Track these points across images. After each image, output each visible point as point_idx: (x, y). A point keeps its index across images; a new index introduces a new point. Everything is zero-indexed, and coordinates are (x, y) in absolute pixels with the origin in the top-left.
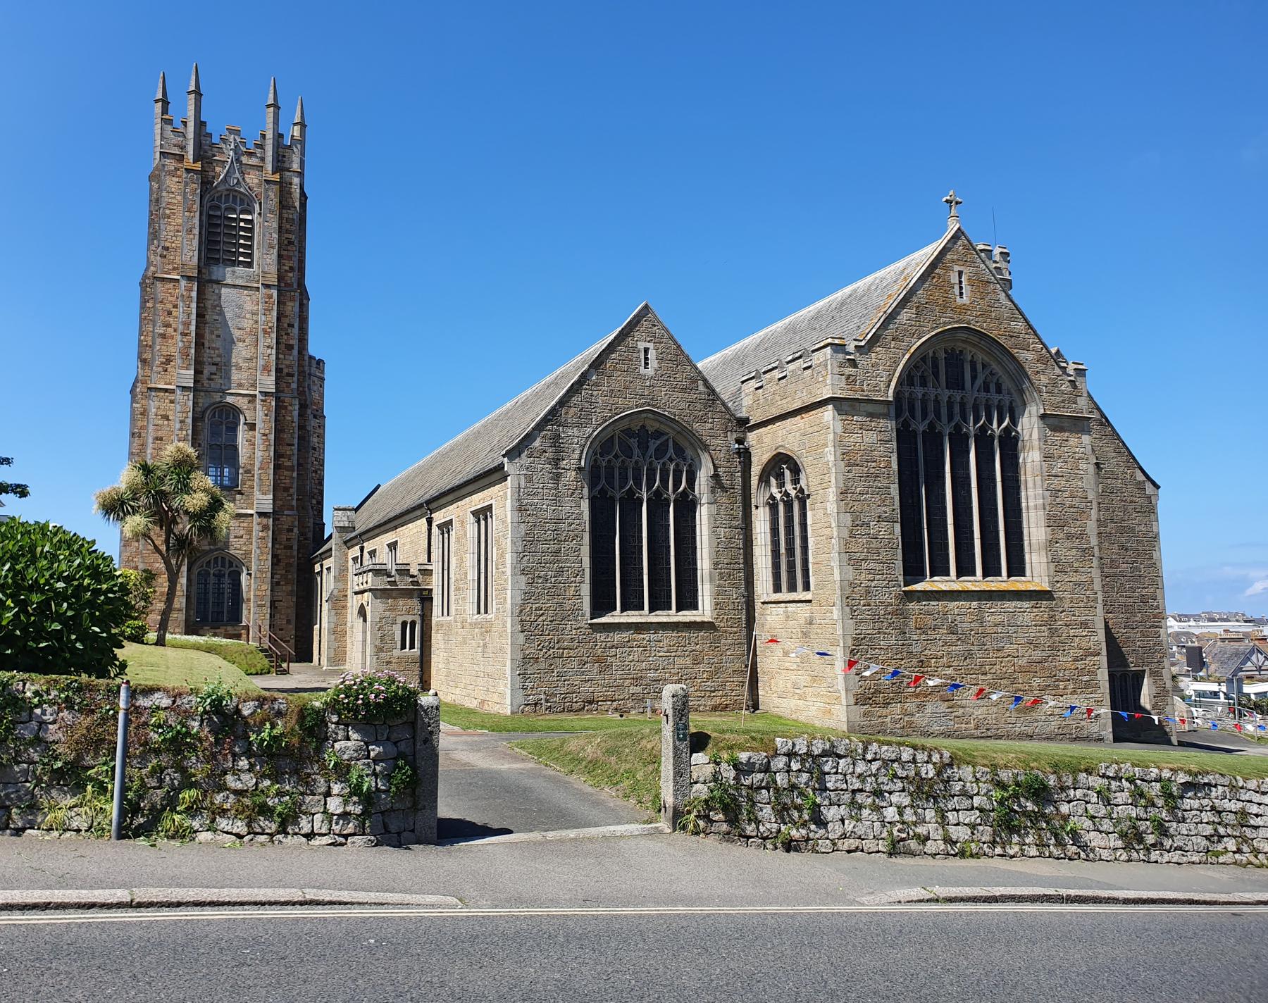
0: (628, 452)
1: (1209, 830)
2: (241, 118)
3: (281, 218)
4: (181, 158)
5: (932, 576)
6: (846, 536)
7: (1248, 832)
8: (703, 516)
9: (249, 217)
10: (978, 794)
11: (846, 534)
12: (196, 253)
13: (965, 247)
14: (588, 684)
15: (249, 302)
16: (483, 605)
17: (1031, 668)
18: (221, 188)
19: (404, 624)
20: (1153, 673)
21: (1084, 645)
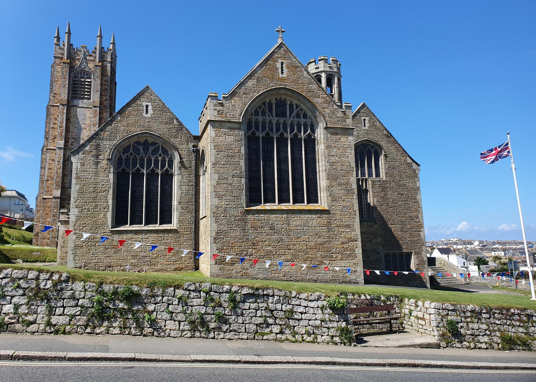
1: (260, 320)
2: (86, 41)
3: (102, 80)
4: (62, 58)
5: (264, 203)
6: (215, 184)
7: (292, 322)
8: (176, 180)
9: (90, 80)
10: (84, 298)
11: (215, 183)
12: (67, 95)
13: (285, 51)
14: (109, 258)
15: (89, 113)
17: (317, 247)
18: (78, 69)
20: (416, 253)
21: (348, 236)
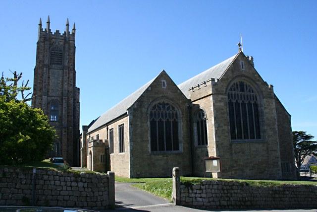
0: (160, 108)
2: (58, 27)
16: (122, 149)
19: (102, 156)
